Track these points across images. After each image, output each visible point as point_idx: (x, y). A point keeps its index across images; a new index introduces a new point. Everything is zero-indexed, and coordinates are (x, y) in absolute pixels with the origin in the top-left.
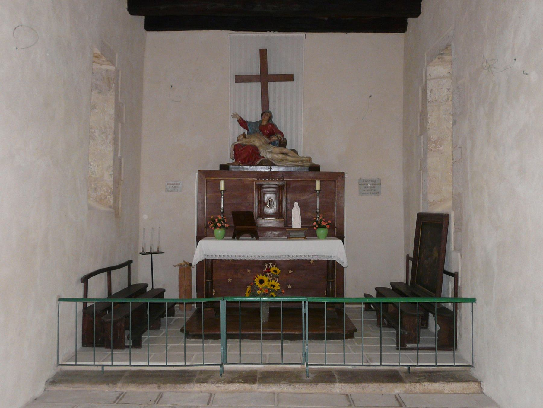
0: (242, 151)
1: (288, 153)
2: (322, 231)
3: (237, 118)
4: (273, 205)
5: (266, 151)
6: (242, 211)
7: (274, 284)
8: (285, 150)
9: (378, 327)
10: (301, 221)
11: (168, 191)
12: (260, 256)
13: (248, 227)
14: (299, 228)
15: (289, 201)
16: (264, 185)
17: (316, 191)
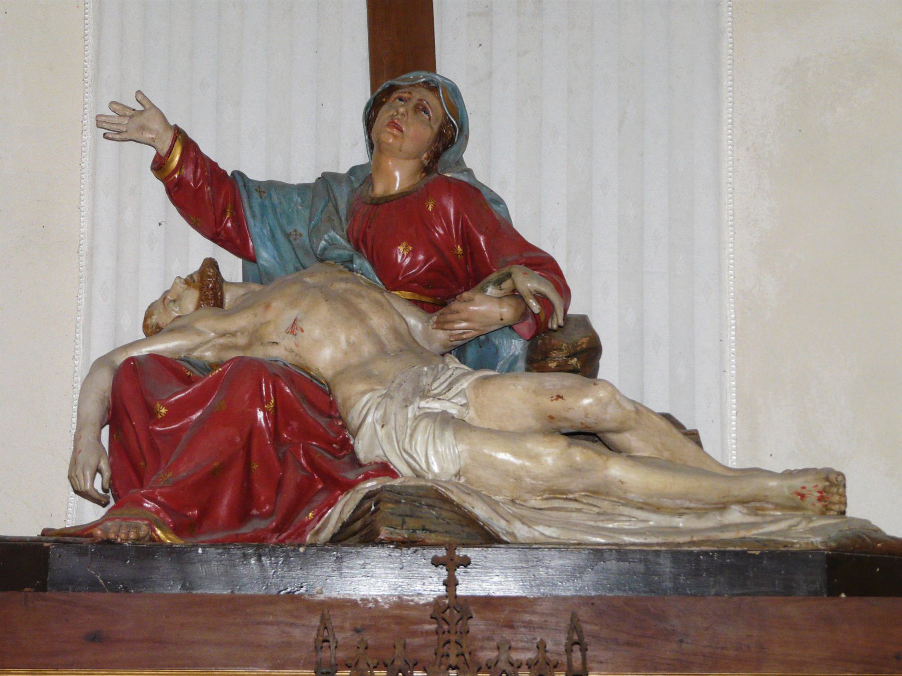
0: (180, 410)
5: (411, 412)
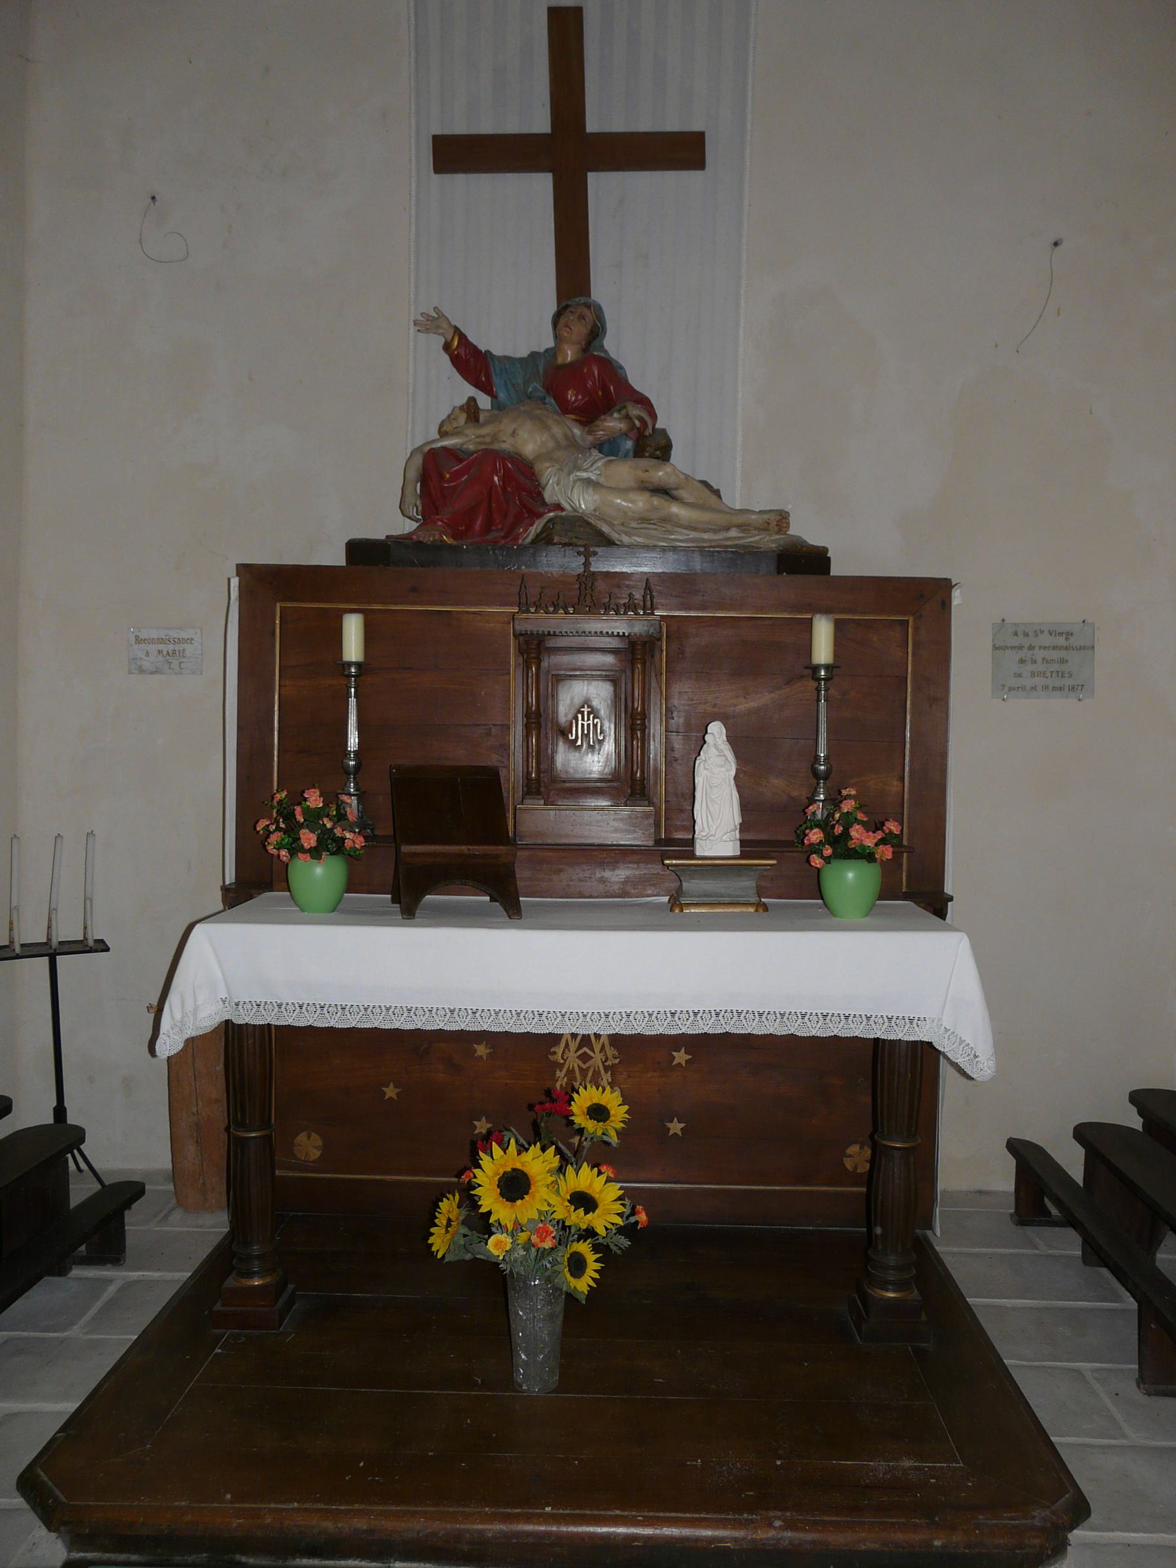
0: (456, 475)
1: (671, 489)
2: (850, 875)
3: (443, 335)
4: (601, 738)
6: (448, 763)
7: (591, 1185)
8: (660, 474)
9: (1149, 1395)
10: (738, 820)
11: (142, 671)
12: (518, 1014)
13: (464, 848)
14: (731, 854)
15: (678, 720)
16: (555, 635)
17: (816, 668)
